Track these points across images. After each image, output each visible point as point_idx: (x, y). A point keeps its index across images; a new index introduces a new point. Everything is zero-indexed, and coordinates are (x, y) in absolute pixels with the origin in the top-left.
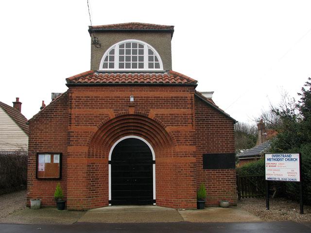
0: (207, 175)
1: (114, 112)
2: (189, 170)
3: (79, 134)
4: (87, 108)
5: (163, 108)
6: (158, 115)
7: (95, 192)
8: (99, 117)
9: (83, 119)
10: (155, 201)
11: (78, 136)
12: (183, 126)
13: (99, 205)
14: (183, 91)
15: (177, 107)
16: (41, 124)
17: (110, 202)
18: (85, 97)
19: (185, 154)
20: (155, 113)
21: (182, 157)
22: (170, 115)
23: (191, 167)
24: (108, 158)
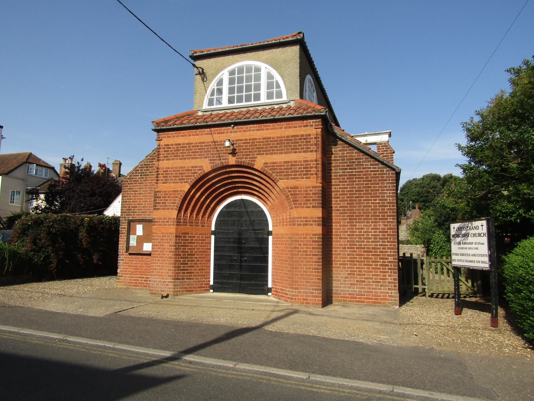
0: (348, 255)
1: (210, 163)
2: (310, 245)
5: (275, 153)
6: (266, 163)
7: (187, 273)
8: (191, 170)
9: (172, 174)
10: (270, 290)
11: (165, 197)
12: (302, 178)
13: (193, 291)
15: (295, 150)
16: (136, 183)
17: (212, 287)
18: (176, 145)
19: (306, 221)
20: (263, 161)
23: (313, 241)
24: (210, 226)
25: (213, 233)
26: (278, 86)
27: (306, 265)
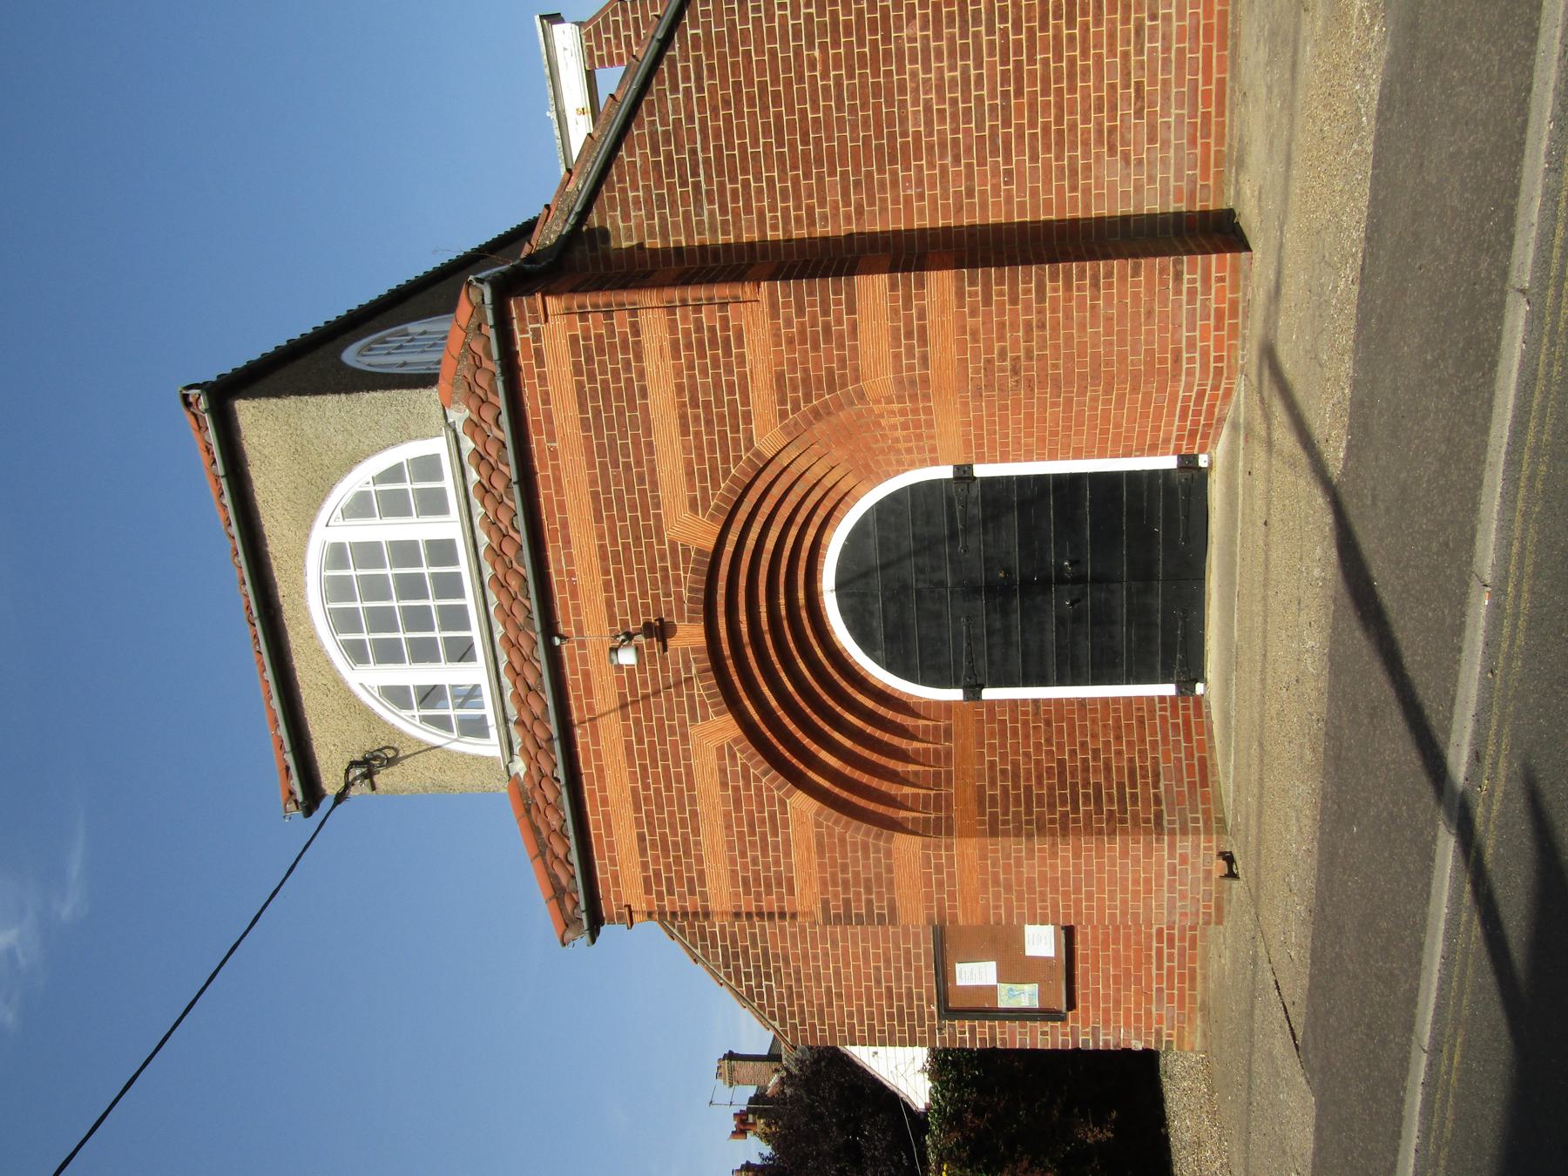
0: (1034, 158)
1: (705, 718)
3: (834, 875)
4: (697, 843)
5: (653, 471)
7: (1133, 785)
9: (755, 861)
10: (1188, 461)
11: (846, 883)
12: (741, 359)
14: (541, 363)
15: (636, 394)
18: (643, 852)
20: (686, 515)
21: (924, 359)
22: (685, 431)
24: (948, 706)
25: (973, 691)
26: (394, 473)
27: (1082, 326)
